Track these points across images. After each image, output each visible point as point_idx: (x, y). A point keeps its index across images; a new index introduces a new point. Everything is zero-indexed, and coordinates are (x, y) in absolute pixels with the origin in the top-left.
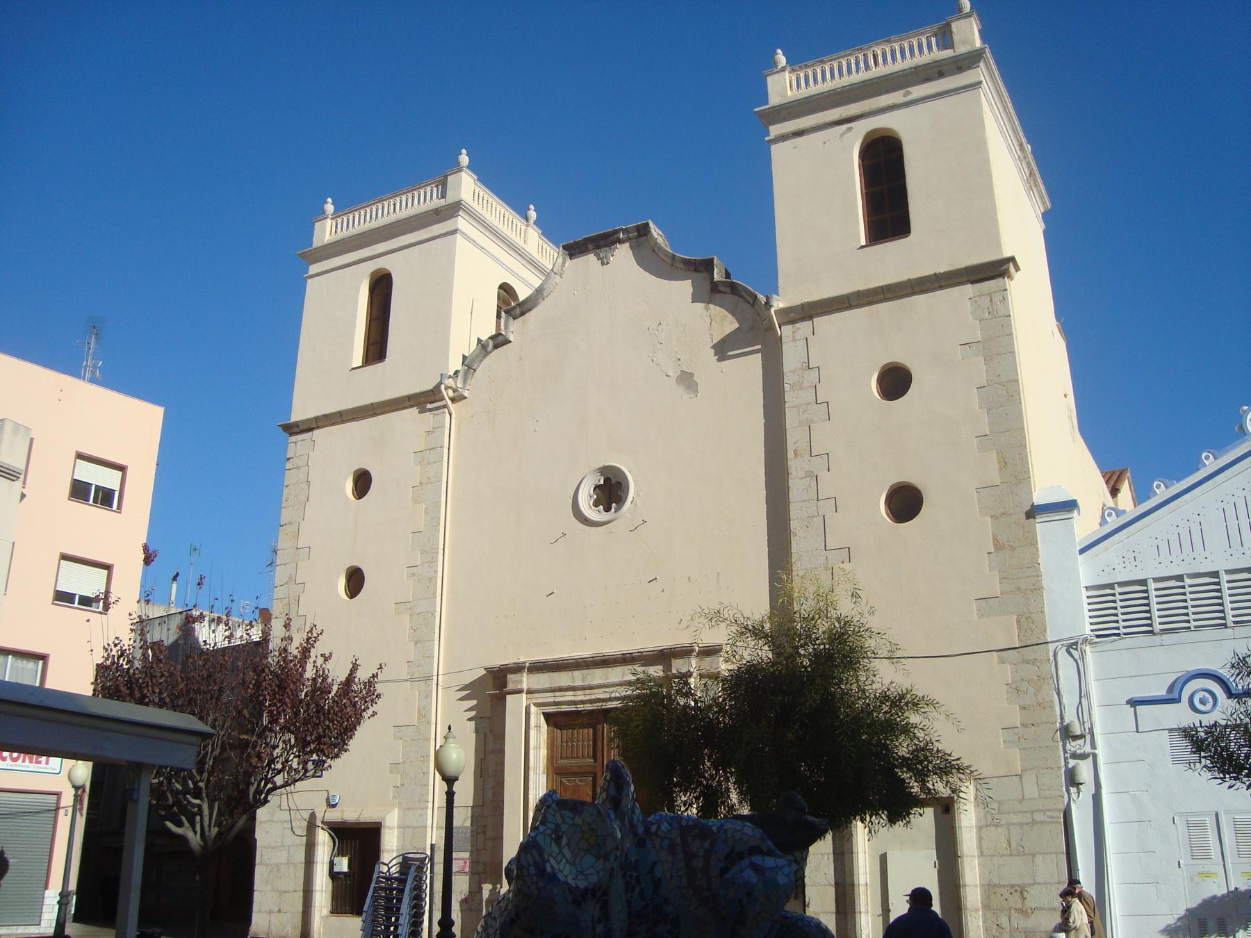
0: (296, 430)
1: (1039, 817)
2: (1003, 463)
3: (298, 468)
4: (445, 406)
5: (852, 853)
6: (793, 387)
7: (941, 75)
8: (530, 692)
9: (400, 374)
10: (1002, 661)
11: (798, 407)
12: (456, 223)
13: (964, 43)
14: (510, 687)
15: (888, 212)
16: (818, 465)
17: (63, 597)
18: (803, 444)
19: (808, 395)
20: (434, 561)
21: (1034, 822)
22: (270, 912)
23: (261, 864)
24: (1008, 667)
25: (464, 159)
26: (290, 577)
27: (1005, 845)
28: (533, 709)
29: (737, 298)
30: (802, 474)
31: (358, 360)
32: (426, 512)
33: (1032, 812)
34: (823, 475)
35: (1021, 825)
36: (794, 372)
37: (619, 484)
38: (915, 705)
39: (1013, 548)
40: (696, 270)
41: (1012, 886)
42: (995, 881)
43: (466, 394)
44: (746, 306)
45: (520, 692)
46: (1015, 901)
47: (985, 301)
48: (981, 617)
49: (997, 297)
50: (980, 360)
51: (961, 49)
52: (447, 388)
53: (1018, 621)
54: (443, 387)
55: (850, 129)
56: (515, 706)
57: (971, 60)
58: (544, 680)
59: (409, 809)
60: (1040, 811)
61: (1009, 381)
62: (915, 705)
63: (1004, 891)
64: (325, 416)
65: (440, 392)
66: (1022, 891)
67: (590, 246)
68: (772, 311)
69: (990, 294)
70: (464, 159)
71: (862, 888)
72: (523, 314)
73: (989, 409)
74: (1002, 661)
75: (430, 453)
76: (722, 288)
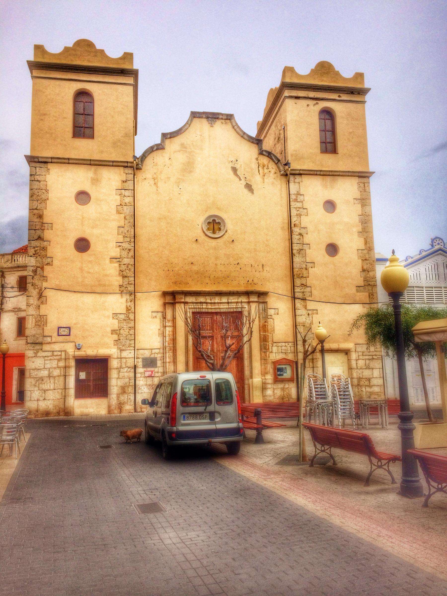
1: (375, 357)
2: (366, 243)
7: (352, 93)
15: (329, 145)
16: (303, 231)
21: (373, 359)
22: (38, 400)
23: (30, 377)
38: (123, 443)
41: (366, 378)
42: (361, 377)
46: (367, 383)
47: (362, 185)
49: (366, 185)
50: (360, 206)
55: (317, 103)
59: (373, 549)
60: (375, 355)
62: (123, 443)
63: (364, 380)
66: (369, 380)
69: (364, 183)
72: (170, 138)
73: (362, 223)
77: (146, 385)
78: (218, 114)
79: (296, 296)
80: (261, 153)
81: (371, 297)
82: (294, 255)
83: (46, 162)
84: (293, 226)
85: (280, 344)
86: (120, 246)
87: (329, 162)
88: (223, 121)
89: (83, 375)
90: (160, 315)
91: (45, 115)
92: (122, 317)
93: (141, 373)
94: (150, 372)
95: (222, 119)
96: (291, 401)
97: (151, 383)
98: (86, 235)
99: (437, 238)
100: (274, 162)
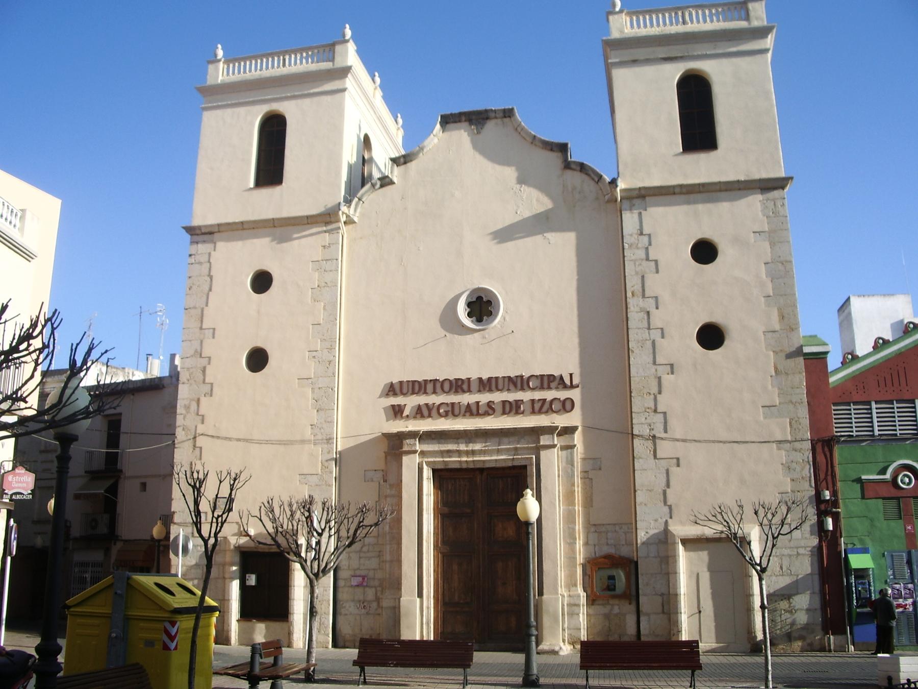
0: (198, 232)
2: (782, 317)
3: (200, 263)
4: (339, 228)
5: (229, 600)
6: (631, 246)
8: (415, 452)
9: (291, 198)
10: (779, 449)
11: (635, 261)
12: (345, 83)
13: (757, 19)
14: (405, 448)
16: (650, 304)
17: (173, 357)
18: (638, 288)
19: (641, 254)
20: (331, 349)
21: (798, 554)
24: (784, 453)
25: (348, 33)
26: (196, 351)
27: (778, 569)
28: (425, 467)
29: (584, 176)
30: (637, 309)
31: (252, 184)
32: (324, 309)
33: (797, 548)
34: (653, 311)
35: (790, 556)
36: (631, 235)
37: (489, 303)
39: (787, 374)
40: (552, 150)
43: (356, 219)
44: (592, 183)
45: (415, 452)
47: (770, 205)
48: (765, 418)
49: (779, 203)
51: (756, 23)
52: (343, 213)
53: (790, 423)
54: (340, 213)
56: (410, 463)
57: (762, 33)
58: (427, 447)
61: (786, 261)
64: (228, 224)
65: (337, 214)
67: (463, 118)
68: (618, 189)
70: (348, 33)
71: (682, 597)
74: (779, 449)
75: (327, 263)
76: (573, 166)
77: (353, 601)
78: (486, 111)
79: (636, 432)
80: (567, 165)
81: (795, 426)
82: (633, 352)
83: (211, 233)
84: (629, 294)
85: (603, 529)
86: (314, 357)
87: (702, 168)
88: (499, 121)
89: (252, 580)
90: (379, 475)
91: (484, 512)
92: (314, 480)
93: (345, 580)
94: (361, 579)
95: (496, 118)
96: (626, 639)
97: (361, 598)
98: (260, 344)
99: (555, 399)
100: (593, 179)
